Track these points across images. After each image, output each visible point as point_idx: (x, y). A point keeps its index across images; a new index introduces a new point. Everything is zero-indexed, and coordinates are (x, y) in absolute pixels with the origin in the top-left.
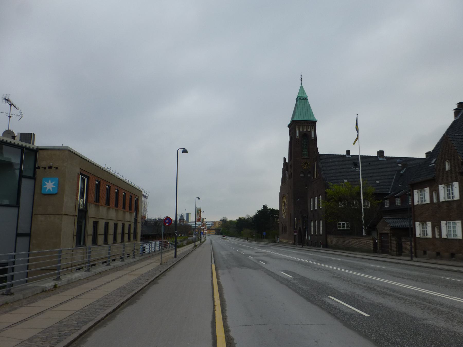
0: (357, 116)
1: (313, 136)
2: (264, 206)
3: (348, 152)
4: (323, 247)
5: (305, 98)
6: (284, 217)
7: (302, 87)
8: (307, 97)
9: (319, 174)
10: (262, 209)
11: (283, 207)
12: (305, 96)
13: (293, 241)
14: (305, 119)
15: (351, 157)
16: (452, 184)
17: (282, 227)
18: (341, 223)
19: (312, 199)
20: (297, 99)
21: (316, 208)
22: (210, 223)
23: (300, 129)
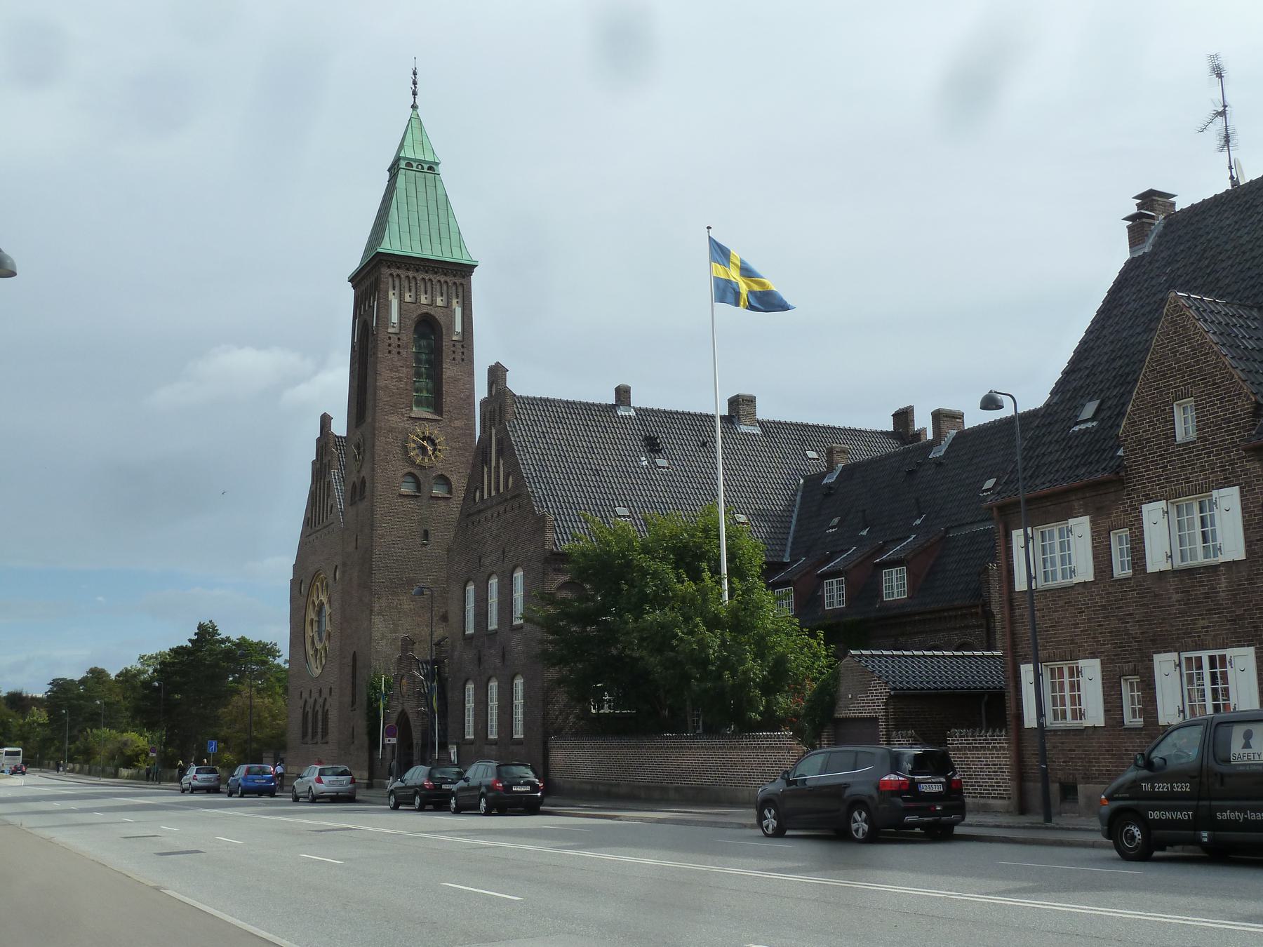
1: (458, 328)
2: (201, 627)
3: (623, 394)
7: (415, 121)
8: (437, 164)
9: (511, 479)
10: (190, 640)
11: (308, 628)
12: (429, 158)
13: (366, 775)
15: (632, 413)
16: (1211, 496)
17: (305, 715)
19: (471, 588)
20: (394, 170)
21: (493, 626)
23: (407, 295)
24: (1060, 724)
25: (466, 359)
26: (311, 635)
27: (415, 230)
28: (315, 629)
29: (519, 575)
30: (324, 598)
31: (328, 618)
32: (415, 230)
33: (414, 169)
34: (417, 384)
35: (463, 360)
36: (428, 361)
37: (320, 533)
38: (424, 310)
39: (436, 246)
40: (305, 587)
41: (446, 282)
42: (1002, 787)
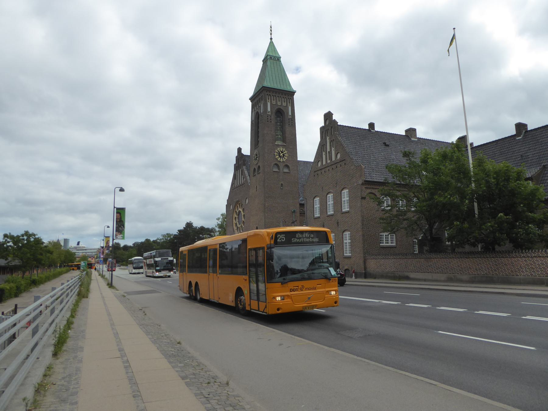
0: (454, 30)
1: (290, 114)
3: (372, 125)
4: (356, 278)
7: (271, 44)
8: (280, 58)
10: (184, 227)
11: (234, 221)
14: (278, 87)
18: (384, 236)
20: (265, 61)
22: (95, 251)
25: (293, 124)
26: (235, 222)
28: (237, 220)
29: (345, 192)
30: (241, 210)
31: (243, 216)
34: (277, 133)
35: (292, 125)
36: (280, 125)
37: (238, 187)
38: (279, 107)
41: (286, 98)
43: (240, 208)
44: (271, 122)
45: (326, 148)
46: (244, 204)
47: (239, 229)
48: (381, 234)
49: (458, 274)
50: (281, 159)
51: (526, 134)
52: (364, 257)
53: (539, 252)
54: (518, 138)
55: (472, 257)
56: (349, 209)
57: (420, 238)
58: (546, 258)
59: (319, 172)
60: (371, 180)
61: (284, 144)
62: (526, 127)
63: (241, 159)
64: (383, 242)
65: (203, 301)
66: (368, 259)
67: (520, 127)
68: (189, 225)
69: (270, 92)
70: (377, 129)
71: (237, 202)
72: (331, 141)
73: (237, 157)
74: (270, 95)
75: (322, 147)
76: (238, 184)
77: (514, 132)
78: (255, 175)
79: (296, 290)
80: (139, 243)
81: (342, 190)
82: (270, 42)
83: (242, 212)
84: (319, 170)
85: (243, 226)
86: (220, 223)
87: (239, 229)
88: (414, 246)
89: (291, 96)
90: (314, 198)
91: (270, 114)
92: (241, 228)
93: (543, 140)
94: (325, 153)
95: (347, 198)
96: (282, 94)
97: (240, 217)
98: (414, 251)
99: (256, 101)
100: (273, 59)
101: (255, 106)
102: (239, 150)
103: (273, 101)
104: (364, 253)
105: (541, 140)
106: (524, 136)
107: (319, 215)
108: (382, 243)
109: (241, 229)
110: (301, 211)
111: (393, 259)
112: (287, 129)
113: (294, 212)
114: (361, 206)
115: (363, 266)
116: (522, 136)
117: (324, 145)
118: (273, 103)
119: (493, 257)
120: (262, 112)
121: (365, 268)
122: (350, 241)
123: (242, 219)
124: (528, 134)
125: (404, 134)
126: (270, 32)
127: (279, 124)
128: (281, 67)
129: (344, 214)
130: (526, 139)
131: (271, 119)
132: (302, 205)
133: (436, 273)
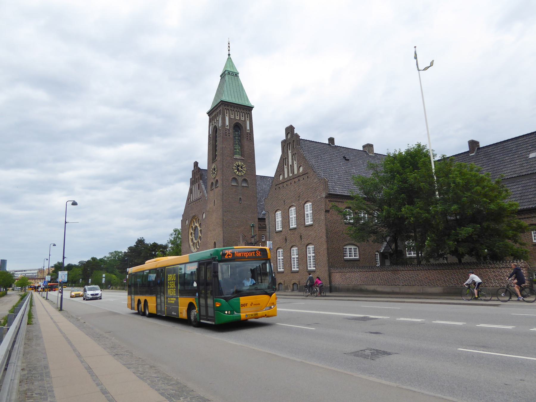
0: (415, 49)
1: (248, 128)
3: (331, 140)
5: (236, 75)
6: (463, 232)
7: (229, 59)
8: (238, 73)
11: (190, 237)
12: (235, 71)
14: (237, 102)
18: (348, 249)
20: (223, 76)
24: (379, 264)
27: (232, 94)
28: (193, 236)
29: (308, 205)
30: (198, 225)
31: (199, 232)
32: (232, 94)
33: (231, 74)
35: (250, 139)
36: (239, 139)
39: (240, 100)
40: (188, 222)
41: (244, 112)
42: (433, 285)
43: (196, 223)
44: (229, 136)
45: (288, 161)
46: (200, 218)
47: (195, 245)
48: (345, 247)
49: (426, 286)
50: (240, 173)
51: (479, 151)
52: (329, 270)
53: (507, 263)
54: (471, 155)
55: (401, 270)
56: (312, 223)
57: (382, 251)
58: (481, 270)
59: (281, 186)
60: (334, 193)
61: (243, 158)
62: (478, 144)
63: (197, 173)
64: (347, 256)
65: (151, 316)
66: (332, 273)
67: (473, 144)
68: (140, 242)
69: (228, 106)
70: (336, 143)
71: (194, 217)
72: (293, 155)
73: (193, 171)
74: (228, 109)
75: (284, 160)
76: (198, 197)
77: (467, 149)
78: (217, 187)
79: (246, 305)
80: (85, 262)
81: (305, 203)
82: (228, 58)
83: (199, 228)
84: (281, 183)
85: (200, 242)
86: (173, 239)
87: (195, 245)
88: (376, 259)
89: (249, 111)
90: (276, 212)
91: (228, 128)
92: (197, 243)
93: (495, 156)
94: (286, 166)
95: (294, 215)
96: (240, 109)
97: (197, 232)
98: (377, 264)
99: (214, 115)
100: (231, 74)
101: (213, 120)
102: (196, 164)
103: (231, 115)
104: (330, 267)
105: (493, 157)
106: (476, 153)
107: (281, 229)
108: (346, 257)
109: (197, 244)
110: (259, 225)
111: (359, 272)
112: (246, 143)
113: (253, 226)
114: (325, 219)
115: (328, 281)
116: (475, 152)
117: (286, 158)
118: (231, 117)
119: (462, 269)
120: (220, 126)
121: (330, 282)
122: (314, 254)
123: (198, 234)
124: (480, 151)
125: (362, 149)
126: (228, 48)
127: (237, 138)
128: (239, 83)
129: (307, 227)
130: (479, 156)
131: (229, 133)
132: (262, 220)
133: (404, 285)
